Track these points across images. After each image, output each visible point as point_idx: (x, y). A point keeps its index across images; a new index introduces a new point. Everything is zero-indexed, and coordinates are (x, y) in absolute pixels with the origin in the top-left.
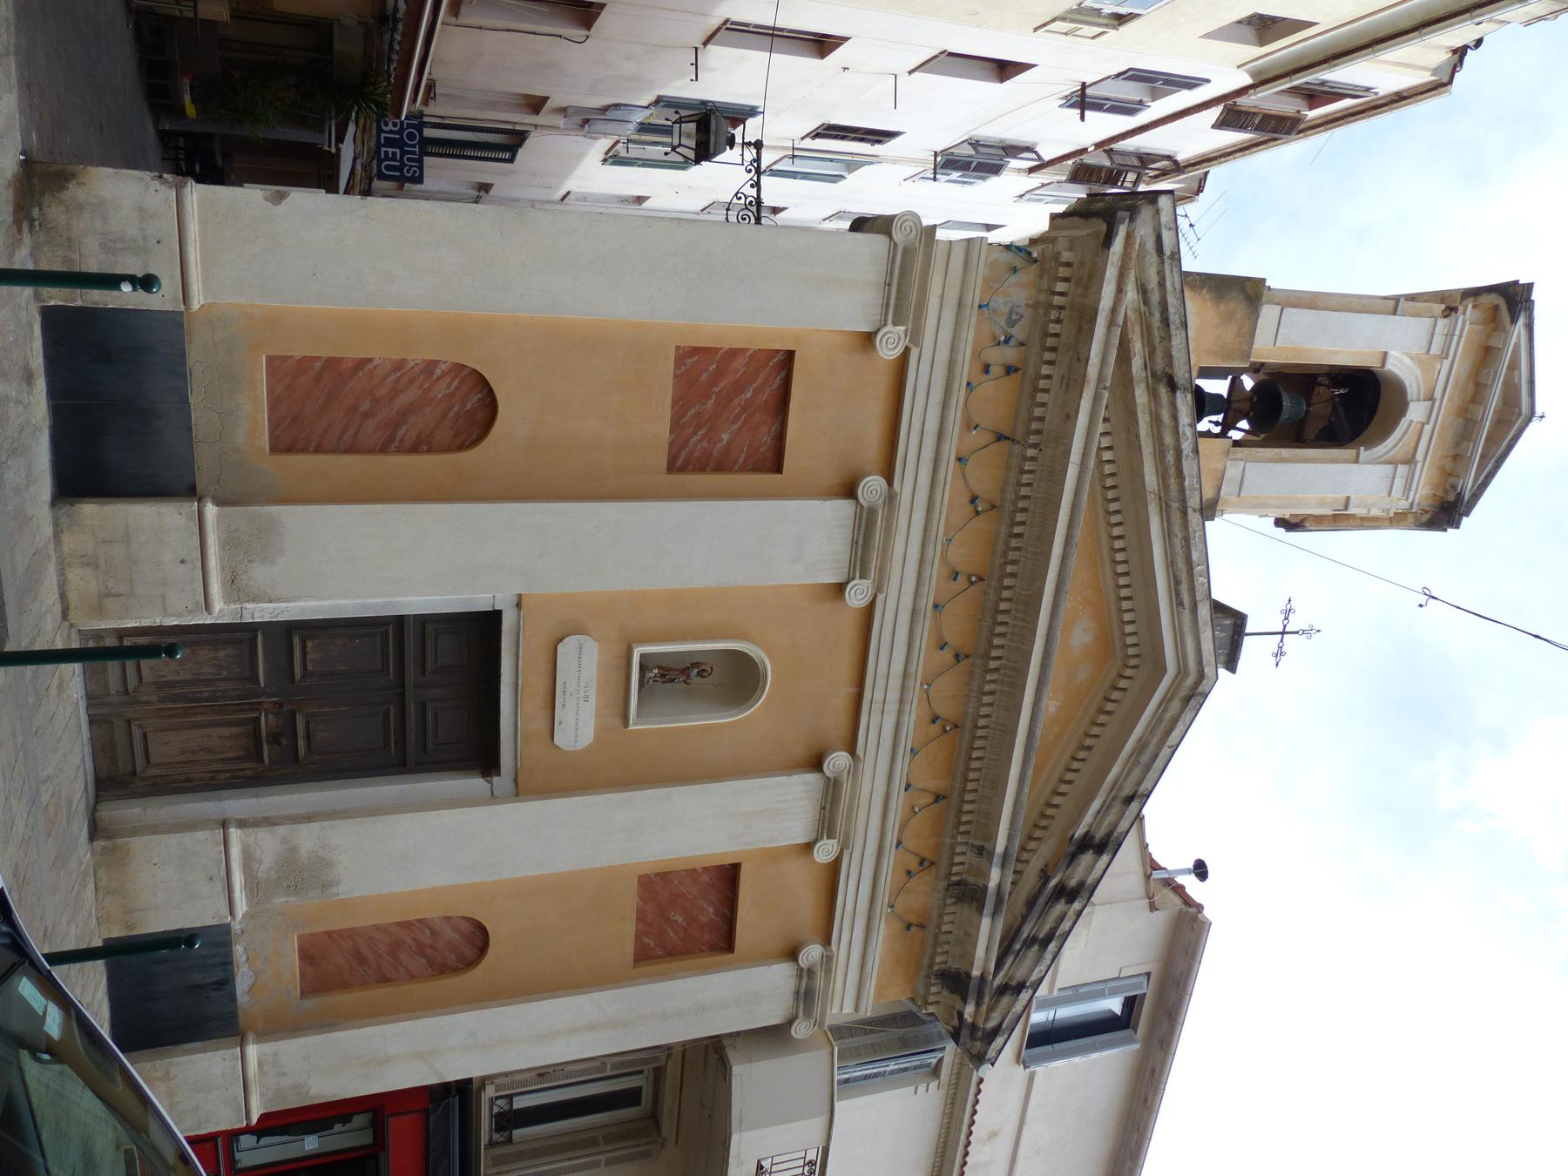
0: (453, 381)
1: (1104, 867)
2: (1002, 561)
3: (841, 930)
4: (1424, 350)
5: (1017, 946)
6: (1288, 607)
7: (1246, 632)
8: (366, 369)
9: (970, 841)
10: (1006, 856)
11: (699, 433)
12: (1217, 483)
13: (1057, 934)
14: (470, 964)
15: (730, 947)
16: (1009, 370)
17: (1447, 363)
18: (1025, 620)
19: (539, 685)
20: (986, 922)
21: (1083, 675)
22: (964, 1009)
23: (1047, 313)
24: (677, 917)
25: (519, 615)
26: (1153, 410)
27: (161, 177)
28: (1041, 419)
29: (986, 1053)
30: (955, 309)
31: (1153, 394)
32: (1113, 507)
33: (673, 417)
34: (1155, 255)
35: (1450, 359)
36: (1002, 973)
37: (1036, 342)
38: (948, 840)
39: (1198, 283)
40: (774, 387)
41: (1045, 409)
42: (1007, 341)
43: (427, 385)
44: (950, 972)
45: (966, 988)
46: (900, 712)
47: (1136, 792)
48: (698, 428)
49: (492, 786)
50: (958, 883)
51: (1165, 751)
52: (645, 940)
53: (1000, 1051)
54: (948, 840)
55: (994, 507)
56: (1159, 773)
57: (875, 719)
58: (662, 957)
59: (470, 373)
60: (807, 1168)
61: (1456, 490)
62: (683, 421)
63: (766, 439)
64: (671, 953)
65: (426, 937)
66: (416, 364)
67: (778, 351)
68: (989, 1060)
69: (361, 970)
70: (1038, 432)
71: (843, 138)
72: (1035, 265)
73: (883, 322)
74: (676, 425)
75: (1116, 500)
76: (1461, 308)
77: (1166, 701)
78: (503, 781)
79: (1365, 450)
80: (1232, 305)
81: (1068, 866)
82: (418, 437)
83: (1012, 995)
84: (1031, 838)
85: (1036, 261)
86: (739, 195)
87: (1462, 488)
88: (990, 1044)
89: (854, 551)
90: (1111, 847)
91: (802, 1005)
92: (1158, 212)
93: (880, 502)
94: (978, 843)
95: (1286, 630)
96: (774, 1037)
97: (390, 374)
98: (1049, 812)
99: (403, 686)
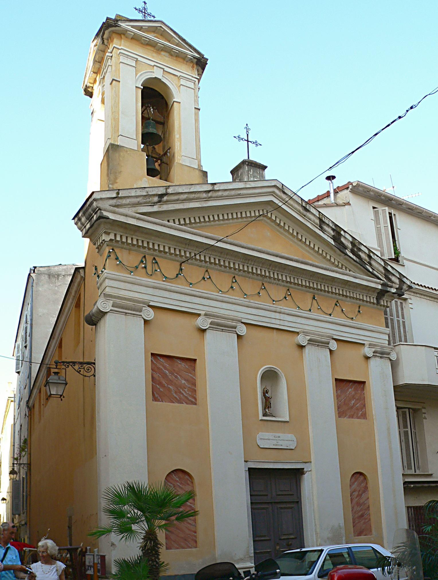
6: (237, 138)
7: (247, 158)
15: (364, 383)
17: (140, 59)
25: (250, 461)
31: (167, 202)
40: (163, 361)
48: (180, 392)
52: (359, 415)
55: (207, 271)
57: (286, 324)
58: (366, 409)
59: (167, 480)
63: (183, 365)
69: (365, 516)
73: (140, 317)
74: (180, 402)
90: (338, 230)
95: (247, 140)
96: (394, 365)
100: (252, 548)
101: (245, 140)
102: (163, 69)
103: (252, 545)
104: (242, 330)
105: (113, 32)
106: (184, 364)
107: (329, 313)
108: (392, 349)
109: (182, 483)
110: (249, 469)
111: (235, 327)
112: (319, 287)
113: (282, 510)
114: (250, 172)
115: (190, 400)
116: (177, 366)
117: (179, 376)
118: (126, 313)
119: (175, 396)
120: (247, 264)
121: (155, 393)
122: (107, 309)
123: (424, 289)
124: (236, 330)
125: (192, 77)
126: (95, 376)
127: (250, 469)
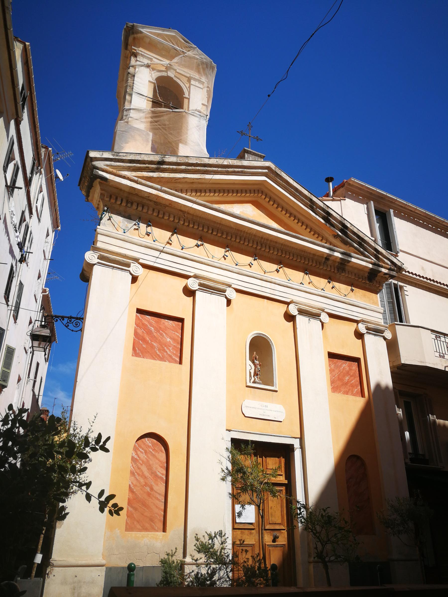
0: (139, 451)
6: (240, 133)
8: (133, 488)
17: (154, 59)
20: (353, 260)
24: (347, 379)
27: (48, 574)
33: (159, 360)
35: (152, 58)
43: (141, 462)
60: (438, 339)
62: (161, 356)
66: (132, 466)
71: (10, 289)
74: (162, 359)
79: (185, 95)
86: (67, 325)
97: (135, 477)
103: (230, 534)
106: (171, 322)
111: (224, 291)
115: (173, 359)
117: (164, 334)
119: (158, 353)
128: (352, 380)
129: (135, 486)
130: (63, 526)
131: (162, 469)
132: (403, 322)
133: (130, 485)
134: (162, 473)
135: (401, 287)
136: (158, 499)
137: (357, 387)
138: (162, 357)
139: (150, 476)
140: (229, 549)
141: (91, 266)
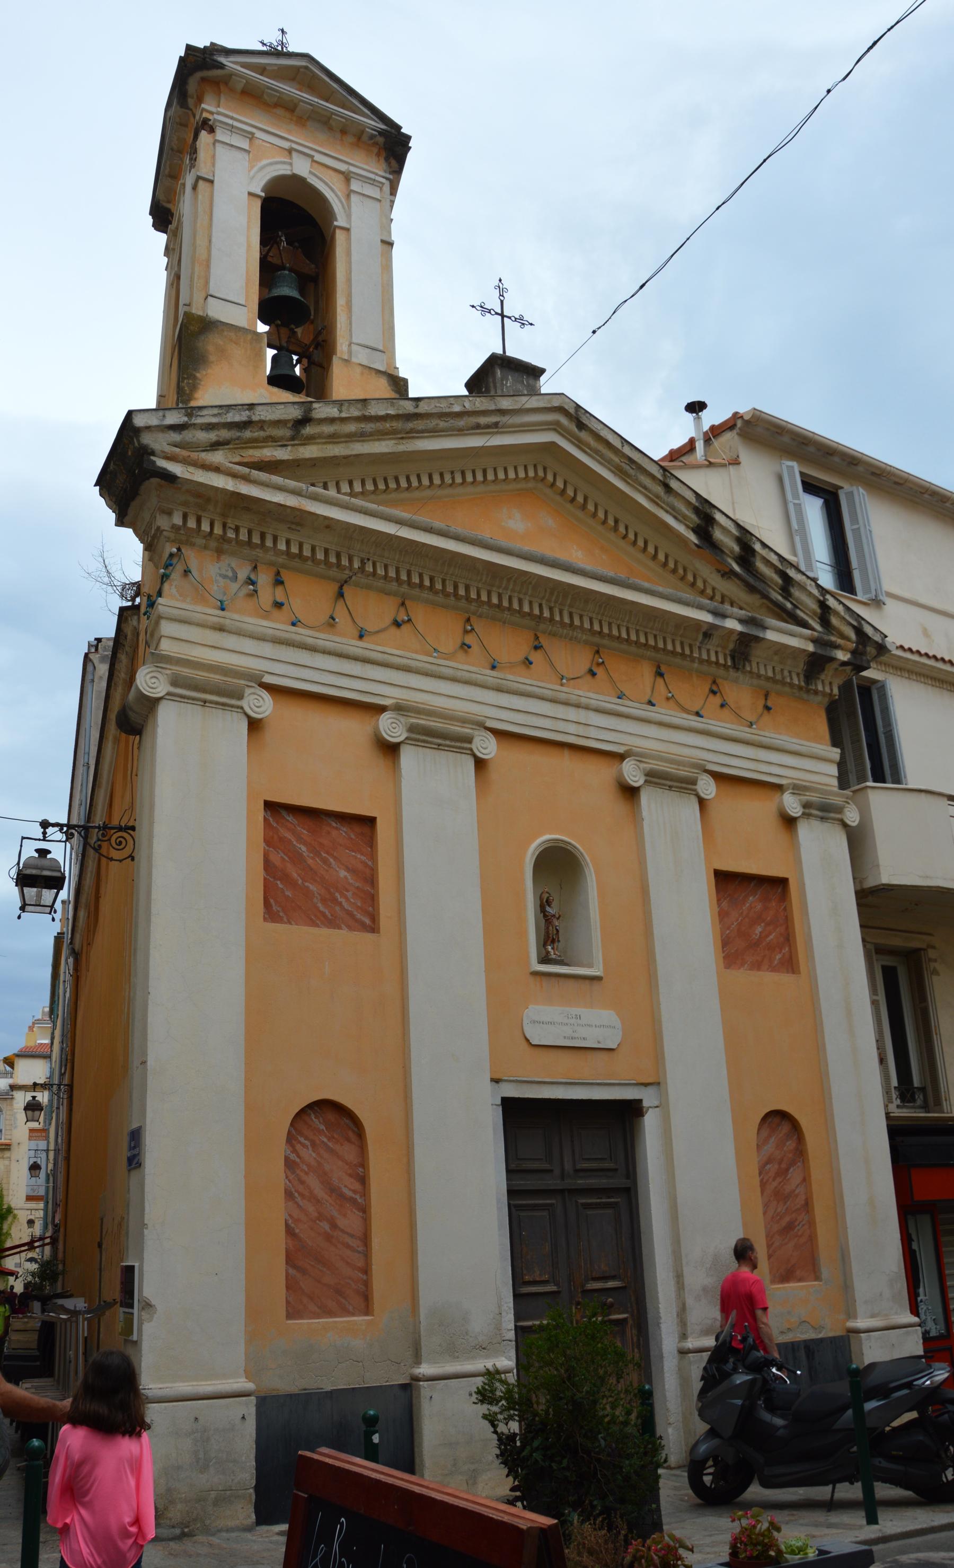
0: (300, 1142)
1: (724, 518)
2: (452, 598)
3: (770, 774)
4: (246, 155)
5: (789, 606)
6: (479, 308)
7: (502, 353)
8: (293, 1225)
9: (698, 644)
10: (715, 613)
11: (339, 900)
12: (374, 374)
13: (781, 567)
14: (795, 1126)
15: (782, 883)
16: (278, 582)
17: (258, 134)
18: (509, 580)
19: (565, 1059)
20: (771, 635)
21: (550, 522)
22: (839, 660)
23: (229, 541)
26: (324, 441)
28: (326, 552)
29: (876, 642)
30: (225, 634)
31: (310, 440)
32: (404, 484)
34: (185, 433)
35: (254, 130)
36: (811, 622)
37: (255, 553)
38: (696, 665)
39: (191, 381)
40: (295, 822)
41: (317, 548)
42: (253, 583)
43: (305, 1168)
44: (806, 671)
45: (822, 656)
46: (587, 708)
47: (660, 481)
48: (335, 900)
49: (651, 1107)
50: (733, 658)
51: (627, 450)
53: (875, 629)
54: (696, 665)
55: (403, 604)
56: (645, 457)
57: (593, 733)
59: (296, 1129)
61: (375, 136)
63: (341, 833)
64: (788, 938)
65: (772, 1168)
67: (265, 819)
68: (883, 640)
69: (798, 1228)
70: (338, 556)
72: (183, 550)
73: (239, 710)
74: (332, 923)
75: (397, 480)
76: (205, 115)
77: (580, 444)
78: (648, 1098)
79: (336, 220)
80: (211, 348)
81: (722, 552)
82: (351, 1176)
83: (829, 613)
84: (693, 585)
85: (179, 549)
87: (375, 130)
88: (869, 638)
89: (446, 748)
91: (832, 815)
92: (148, 428)
93: (403, 719)
94: (700, 637)
95: (500, 312)
97: (296, 1203)
98: (671, 565)
99: (562, 1191)
100: (511, 1316)
101: (497, 313)
102: (312, 157)
103: (510, 1308)
104: (487, 747)
105: (203, 79)
107: (695, 710)
108: (847, 798)
109: (334, 1138)
110: (504, 1100)
111: (469, 740)
112: (670, 647)
113: (590, 1212)
114: (507, 383)
115: (357, 920)
116: (329, 833)
117: (331, 860)
118: (205, 702)
119: (322, 908)
120: (499, 587)
121: (272, 901)
122: (157, 690)
123: (916, 658)
124: (474, 747)
125: (377, 174)
126: (133, 859)
127: (504, 1100)
128: (770, 934)
129: (297, 1221)
130: (156, 1316)
131: (352, 1180)
132: (904, 783)
133: (286, 1220)
134: (353, 1188)
135: (882, 688)
136: (348, 1246)
137: (781, 949)
138: (330, 917)
139: (327, 1197)
140: (510, 1341)
141: (152, 703)
